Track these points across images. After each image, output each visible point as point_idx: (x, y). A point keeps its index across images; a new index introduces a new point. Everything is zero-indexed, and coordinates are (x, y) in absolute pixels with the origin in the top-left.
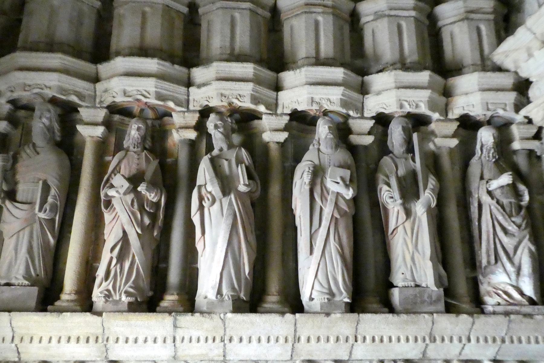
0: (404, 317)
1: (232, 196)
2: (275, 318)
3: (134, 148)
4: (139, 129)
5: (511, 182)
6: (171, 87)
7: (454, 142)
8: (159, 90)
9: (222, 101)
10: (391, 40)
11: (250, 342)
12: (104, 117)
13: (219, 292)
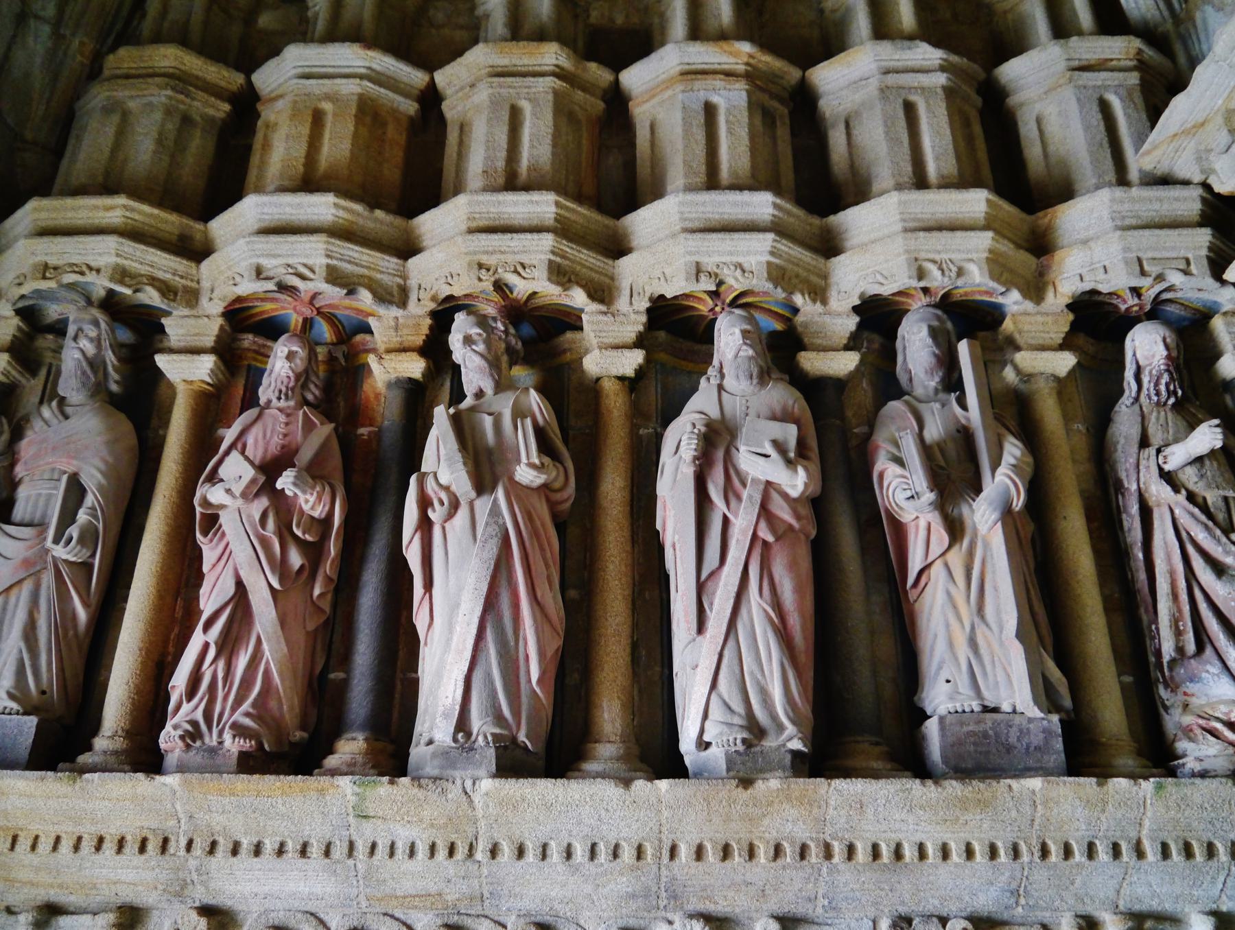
0: (953, 787)
1: (500, 493)
2: (609, 791)
3: (279, 399)
4: (290, 356)
5: (1219, 444)
6: (365, 258)
7: (1065, 362)
8: (335, 262)
9: (480, 280)
10: (892, 140)
11: (544, 856)
12: (218, 336)
13: (462, 724)
